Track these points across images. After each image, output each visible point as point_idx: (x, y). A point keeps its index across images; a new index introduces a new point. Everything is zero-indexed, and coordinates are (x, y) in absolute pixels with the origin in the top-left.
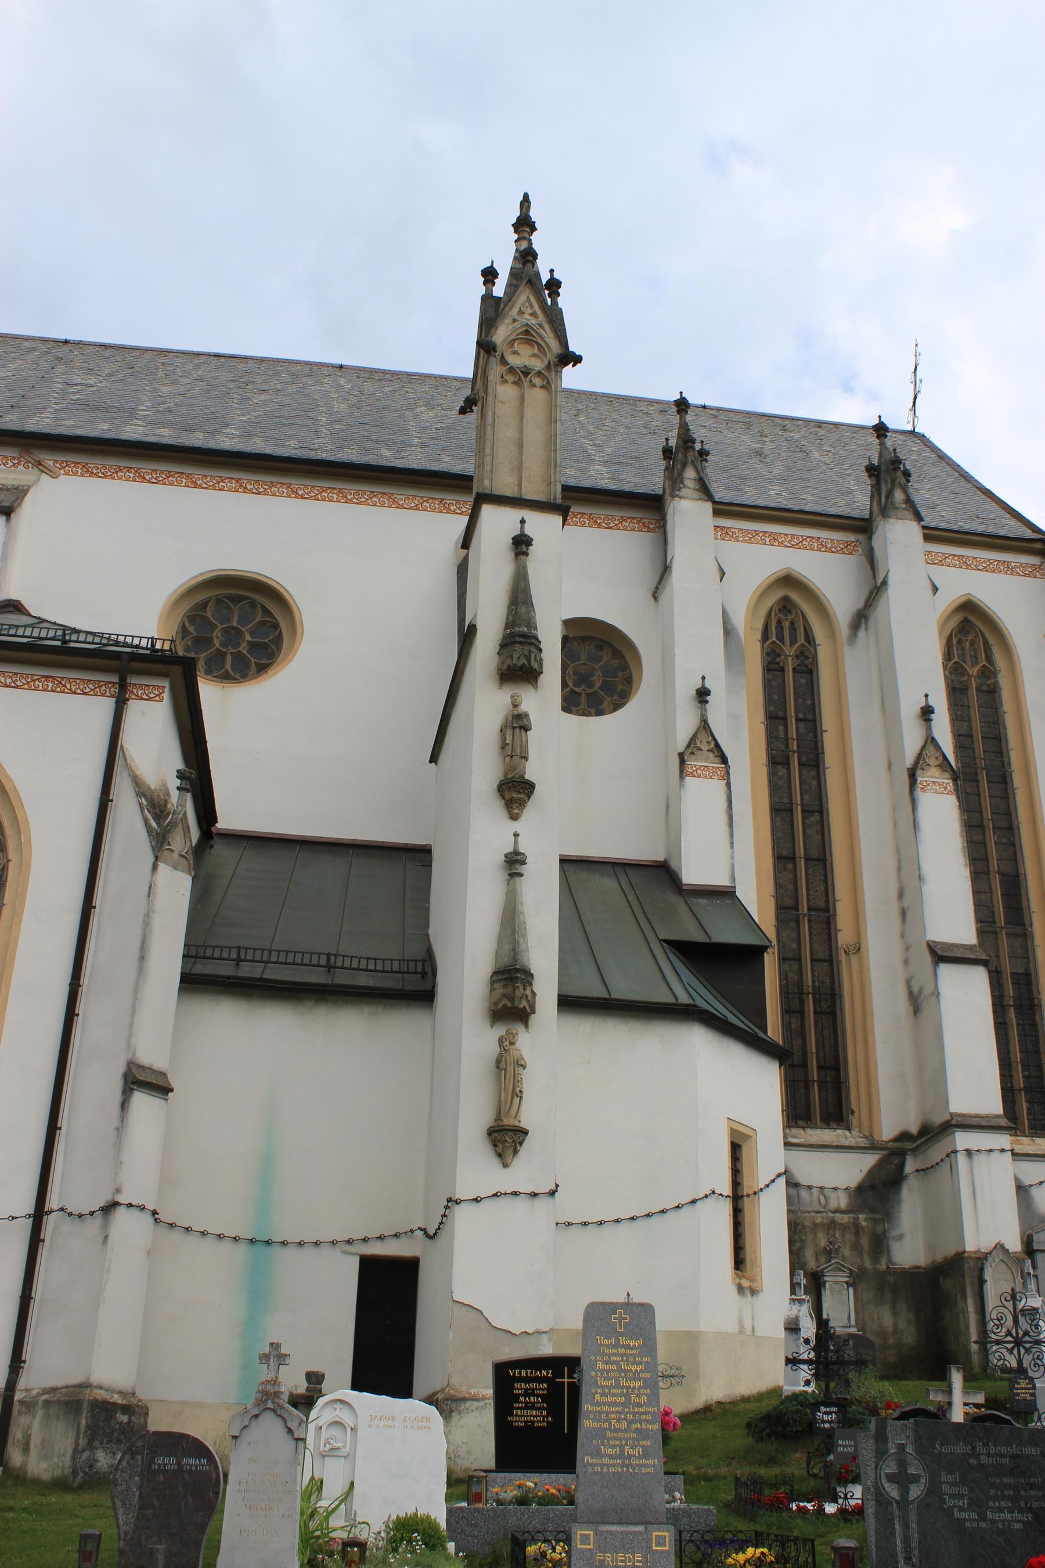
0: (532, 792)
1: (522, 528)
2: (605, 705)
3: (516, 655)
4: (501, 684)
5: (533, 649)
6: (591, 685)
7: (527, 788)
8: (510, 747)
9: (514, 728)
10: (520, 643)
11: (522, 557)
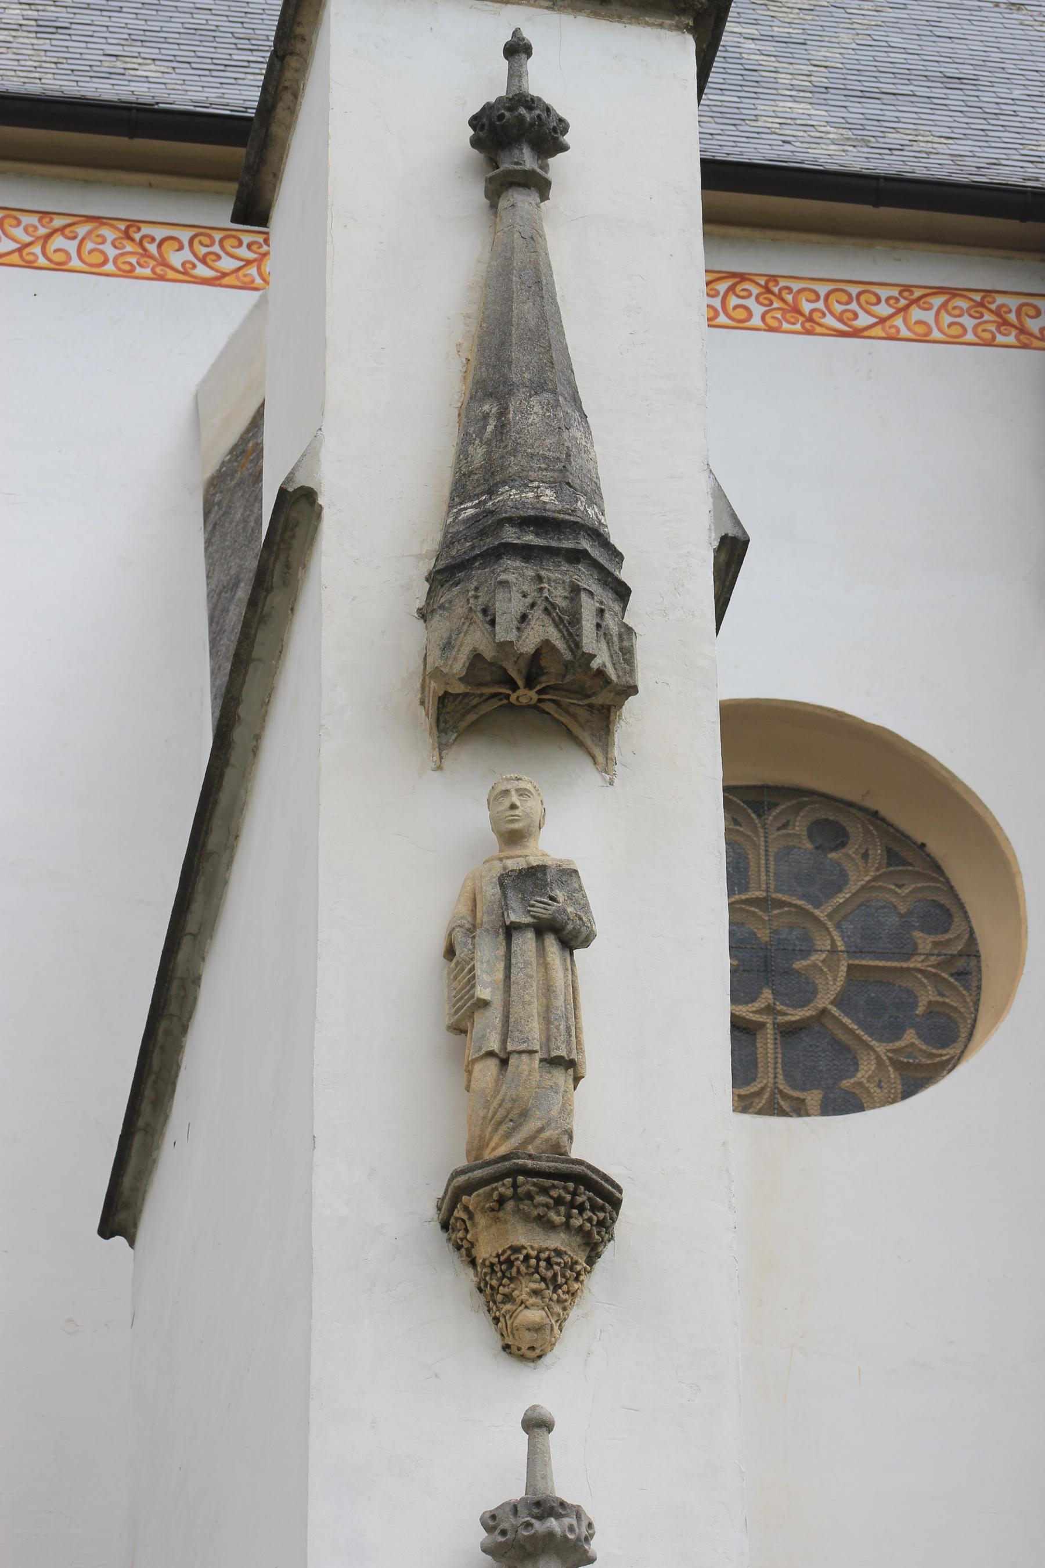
0: (606, 1226)
1: (515, 75)
2: (866, 1069)
3: (509, 606)
4: (442, 747)
5: (587, 580)
6: (806, 994)
7: (586, 1203)
8: (494, 1015)
9: (510, 931)
10: (527, 553)
11: (523, 200)
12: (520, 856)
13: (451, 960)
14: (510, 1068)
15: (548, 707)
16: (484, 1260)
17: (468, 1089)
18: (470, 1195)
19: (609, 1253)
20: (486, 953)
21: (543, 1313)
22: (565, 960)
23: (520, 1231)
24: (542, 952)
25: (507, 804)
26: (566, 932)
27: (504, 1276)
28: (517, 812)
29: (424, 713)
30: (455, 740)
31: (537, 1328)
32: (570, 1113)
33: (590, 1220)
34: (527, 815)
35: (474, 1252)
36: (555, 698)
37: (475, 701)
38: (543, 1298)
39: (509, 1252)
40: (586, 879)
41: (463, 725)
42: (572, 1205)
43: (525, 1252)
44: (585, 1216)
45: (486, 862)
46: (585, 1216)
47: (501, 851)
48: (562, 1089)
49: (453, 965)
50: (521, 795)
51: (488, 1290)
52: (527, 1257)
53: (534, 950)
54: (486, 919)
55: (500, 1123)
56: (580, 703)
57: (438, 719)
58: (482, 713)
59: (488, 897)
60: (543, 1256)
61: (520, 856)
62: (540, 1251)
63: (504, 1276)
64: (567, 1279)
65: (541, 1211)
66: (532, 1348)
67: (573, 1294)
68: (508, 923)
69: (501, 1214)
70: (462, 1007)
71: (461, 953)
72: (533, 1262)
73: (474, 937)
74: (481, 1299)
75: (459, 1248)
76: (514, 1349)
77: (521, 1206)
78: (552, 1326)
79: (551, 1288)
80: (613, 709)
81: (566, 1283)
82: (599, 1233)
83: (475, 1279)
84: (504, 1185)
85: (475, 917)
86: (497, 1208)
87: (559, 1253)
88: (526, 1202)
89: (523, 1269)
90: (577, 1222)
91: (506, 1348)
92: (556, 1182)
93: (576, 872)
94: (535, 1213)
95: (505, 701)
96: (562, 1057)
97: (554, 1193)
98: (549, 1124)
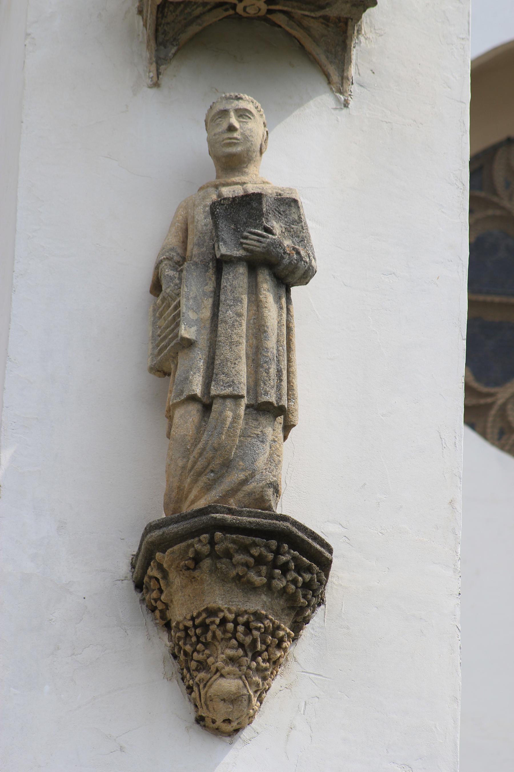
9: (220, 265)
12: (237, 184)
13: (158, 296)
14: (213, 415)
15: (280, 19)
16: (178, 623)
17: (169, 435)
18: (164, 552)
19: (318, 621)
20: (194, 288)
21: (241, 682)
22: (161, 273)
23: (217, 592)
24: (254, 290)
25: (225, 126)
26: (282, 267)
27: (198, 641)
28: (235, 135)
29: (141, 23)
30: (175, 54)
31: (233, 699)
32: (278, 464)
33: (294, 582)
34: (246, 138)
35: (169, 614)
36: (285, 9)
37: (199, 11)
38: (240, 666)
39: (204, 615)
40: (309, 210)
41: (184, 37)
42: (274, 565)
43: (221, 615)
44: (289, 578)
45: (201, 189)
46: (289, 578)
47: (218, 177)
48: (270, 437)
49: (159, 301)
50: (240, 116)
51: (182, 657)
52: (224, 621)
53: (246, 286)
54: (196, 251)
55: (200, 474)
56: (313, 14)
57: (157, 30)
58: (205, 24)
59: (200, 227)
60: (241, 619)
61: (237, 184)
62: (238, 615)
63: (198, 641)
64: (268, 646)
65: (240, 570)
66: (228, 721)
67: (275, 663)
68: (218, 256)
69: (197, 573)
70: (166, 347)
71: (167, 289)
72: (230, 626)
73: (181, 271)
74: (173, 666)
75: (153, 609)
76: (208, 722)
77: (219, 565)
78: (250, 696)
79: (250, 655)
80: (350, 23)
81: (267, 650)
82: (305, 596)
83: (169, 644)
84: (200, 541)
85: (185, 249)
86: (192, 566)
87: (259, 617)
88: (224, 560)
89: (219, 633)
90: (279, 584)
91: (200, 720)
92: (257, 539)
93: (295, 201)
94: (233, 573)
95: (231, 12)
96: (271, 403)
97: (255, 551)
98: (252, 475)
